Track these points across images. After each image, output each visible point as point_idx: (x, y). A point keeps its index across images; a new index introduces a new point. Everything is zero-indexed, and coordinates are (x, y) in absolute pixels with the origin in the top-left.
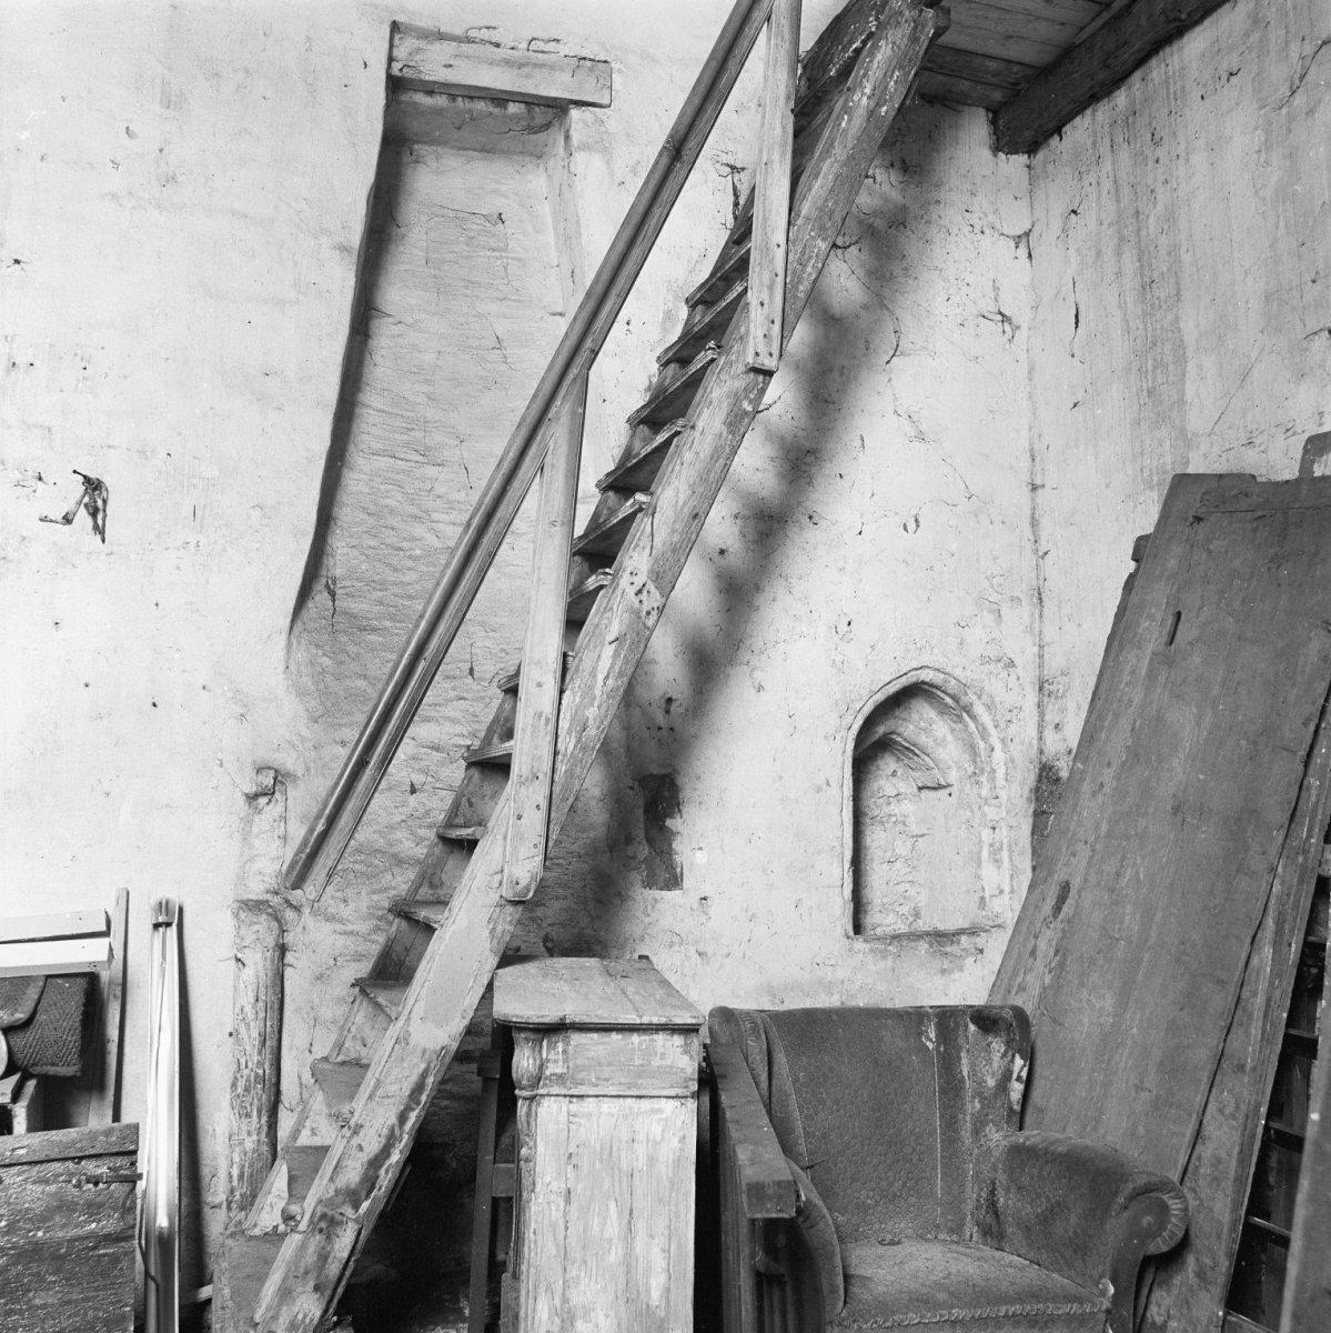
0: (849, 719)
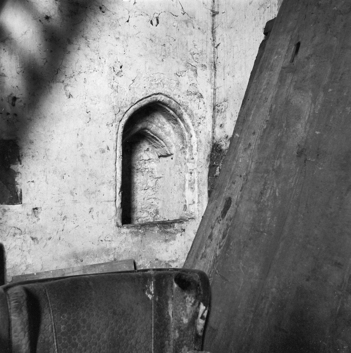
0: (120, 116)
